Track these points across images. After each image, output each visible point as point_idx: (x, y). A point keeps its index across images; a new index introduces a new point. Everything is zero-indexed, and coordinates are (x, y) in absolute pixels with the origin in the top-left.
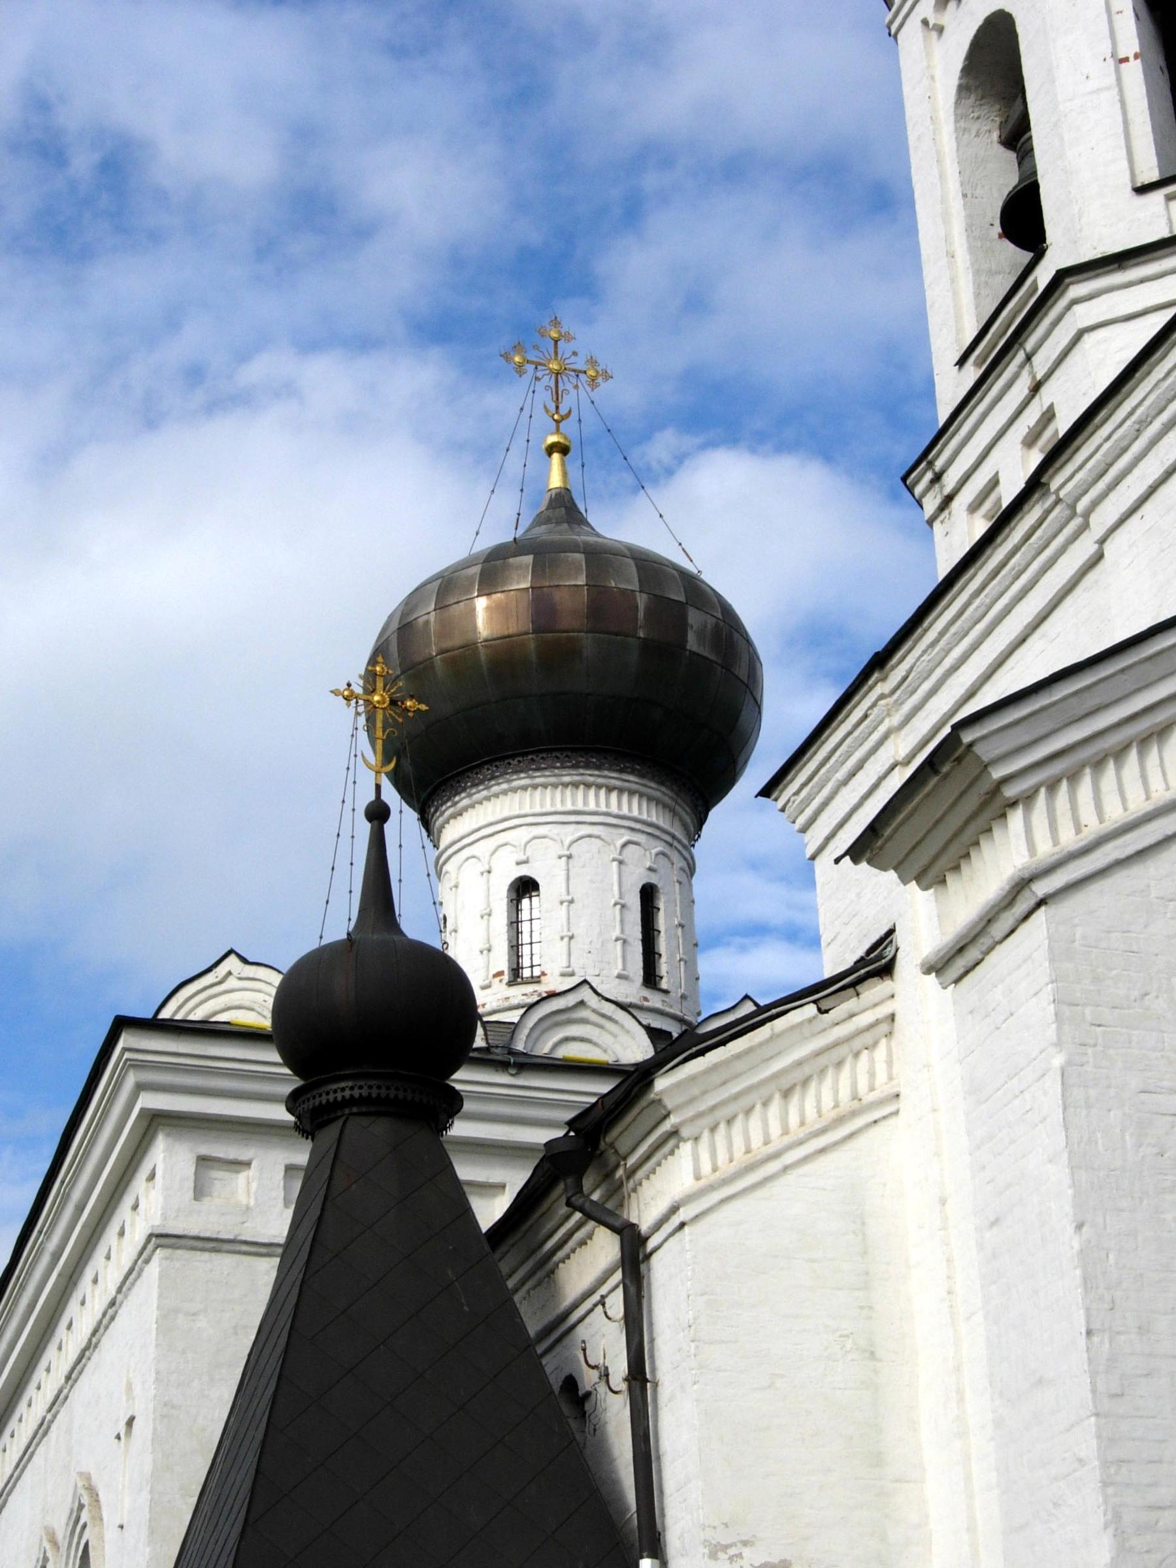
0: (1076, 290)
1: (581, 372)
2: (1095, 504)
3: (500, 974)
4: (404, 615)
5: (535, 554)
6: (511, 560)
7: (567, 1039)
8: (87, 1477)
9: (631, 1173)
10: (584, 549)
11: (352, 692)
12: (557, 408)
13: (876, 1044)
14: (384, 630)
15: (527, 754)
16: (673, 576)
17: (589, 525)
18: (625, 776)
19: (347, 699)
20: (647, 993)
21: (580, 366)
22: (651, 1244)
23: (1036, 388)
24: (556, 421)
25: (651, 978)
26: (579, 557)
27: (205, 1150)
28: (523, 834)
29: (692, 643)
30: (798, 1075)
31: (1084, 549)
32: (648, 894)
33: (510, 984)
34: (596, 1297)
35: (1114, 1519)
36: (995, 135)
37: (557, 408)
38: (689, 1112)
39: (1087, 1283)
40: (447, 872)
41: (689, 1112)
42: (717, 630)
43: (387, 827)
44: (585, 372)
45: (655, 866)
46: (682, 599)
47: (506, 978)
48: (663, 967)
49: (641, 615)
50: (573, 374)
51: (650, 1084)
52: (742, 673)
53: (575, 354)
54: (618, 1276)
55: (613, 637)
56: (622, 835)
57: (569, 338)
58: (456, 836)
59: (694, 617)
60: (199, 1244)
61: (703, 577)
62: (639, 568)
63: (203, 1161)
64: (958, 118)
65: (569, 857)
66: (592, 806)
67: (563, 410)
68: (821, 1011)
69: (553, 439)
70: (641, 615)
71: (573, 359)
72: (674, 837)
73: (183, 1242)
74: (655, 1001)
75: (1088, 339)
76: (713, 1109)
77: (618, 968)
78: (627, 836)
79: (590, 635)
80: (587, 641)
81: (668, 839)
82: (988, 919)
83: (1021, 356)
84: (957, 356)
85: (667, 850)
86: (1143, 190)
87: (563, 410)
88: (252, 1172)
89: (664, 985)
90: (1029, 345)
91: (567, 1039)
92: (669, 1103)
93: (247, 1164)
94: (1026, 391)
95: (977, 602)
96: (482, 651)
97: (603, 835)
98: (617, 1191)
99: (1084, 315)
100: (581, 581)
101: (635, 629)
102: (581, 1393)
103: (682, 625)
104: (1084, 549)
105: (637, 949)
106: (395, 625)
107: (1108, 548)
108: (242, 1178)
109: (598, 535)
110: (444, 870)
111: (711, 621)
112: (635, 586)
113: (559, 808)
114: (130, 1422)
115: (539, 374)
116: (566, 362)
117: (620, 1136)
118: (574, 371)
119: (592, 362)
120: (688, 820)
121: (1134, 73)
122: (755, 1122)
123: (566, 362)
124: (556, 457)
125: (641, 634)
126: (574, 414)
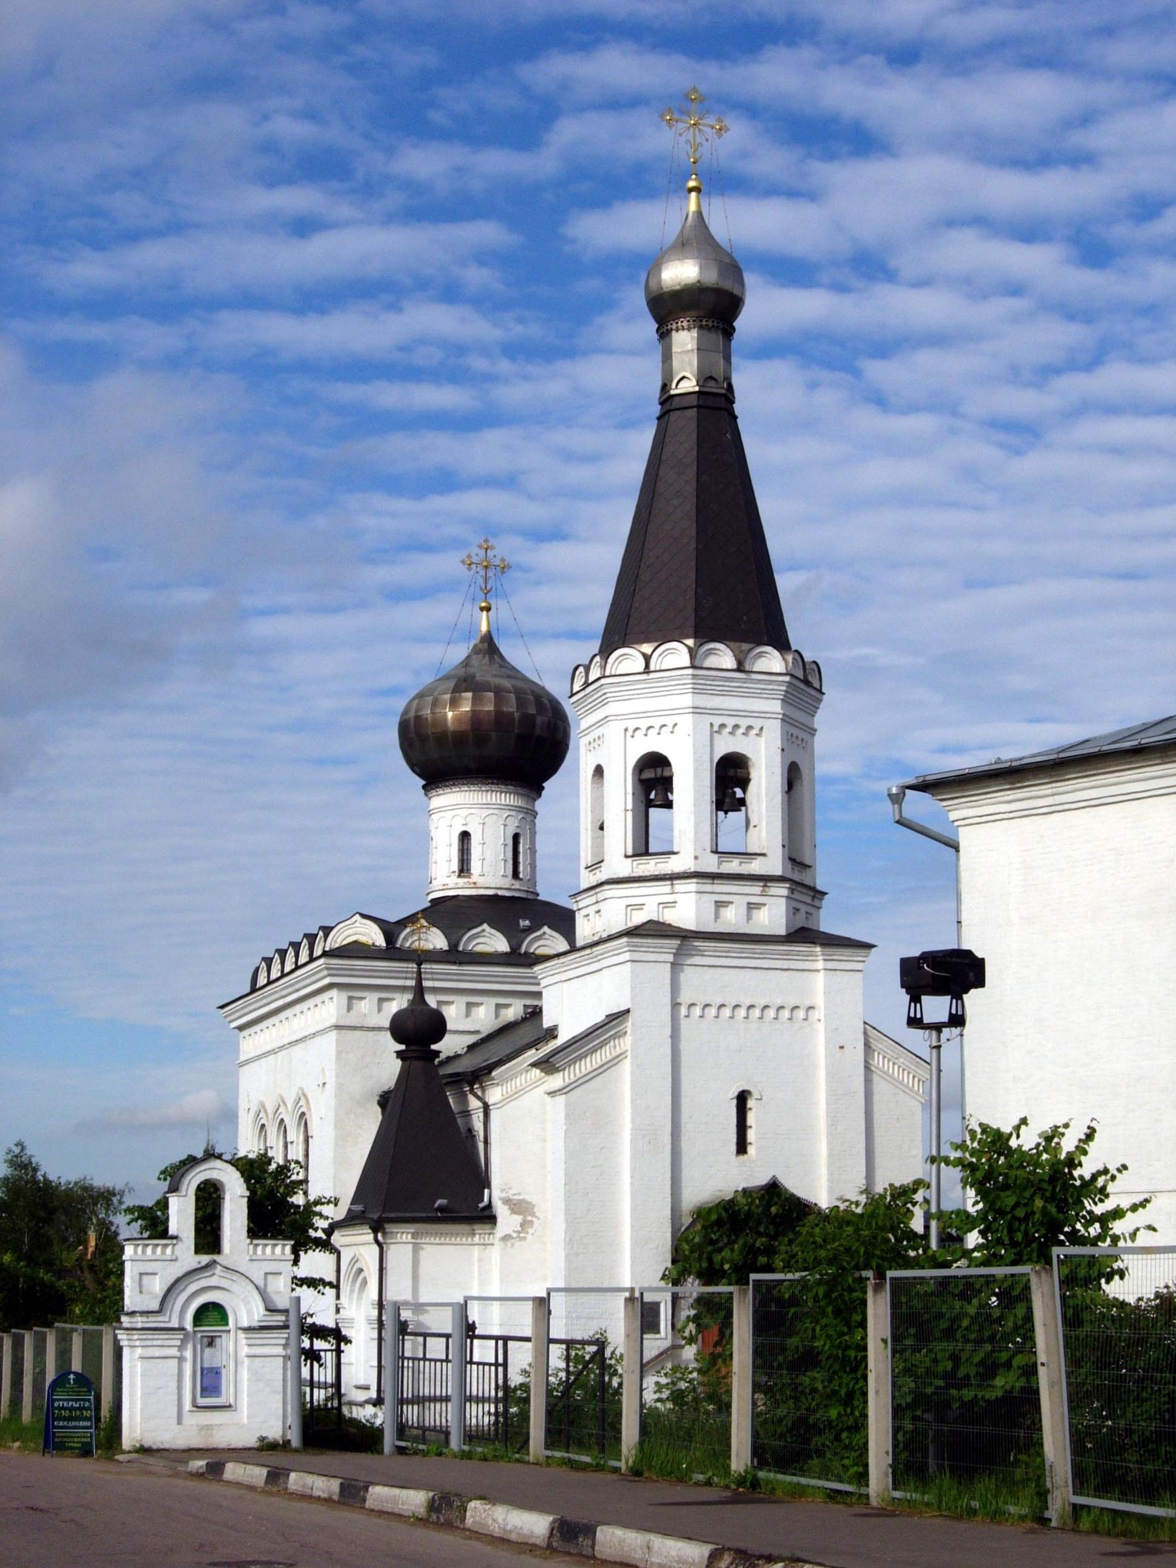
3: (454, 872)
6: (463, 694)
7: (478, 944)
8: (302, 1089)
10: (495, 687)
20: (513, 882)
25: (516, 874)
26: (491, 695)
27: (351, 994)
28: (465, 812)
29: (538, 732)
32: (516, 837)
33: (459, 876)
35: (567, 1220)
39: (566, 1174)
46: (534, 712)
47: (457, 874)
48: (521, 868)
49: (516, 723)
57: (492, 548)
62: (517, 699)
63: (350, 998)
64: (592, 783)
65: (484, 824)
66: (494, 801)
67: (488, 588)
69: (483, 604)
70: (516, 723)
74: (517, 885)
77: (502, 872)
78: (508, 813)
86: (626, 856)
87: (488, 588)
88: (367, 1001)
89: (521, 876)
91: (478, 944)
93: (365, 998)
96: (450, 739)
99: (608, 894)
100: (492, 708)
105: (510, 862)
108: (363, 1003)
111: (546, 719)
113: (480, 802)
119: (503, 560)
121: (630, 815)
122: (518, 1079)
124: (485, 613)
126: (493, 589)
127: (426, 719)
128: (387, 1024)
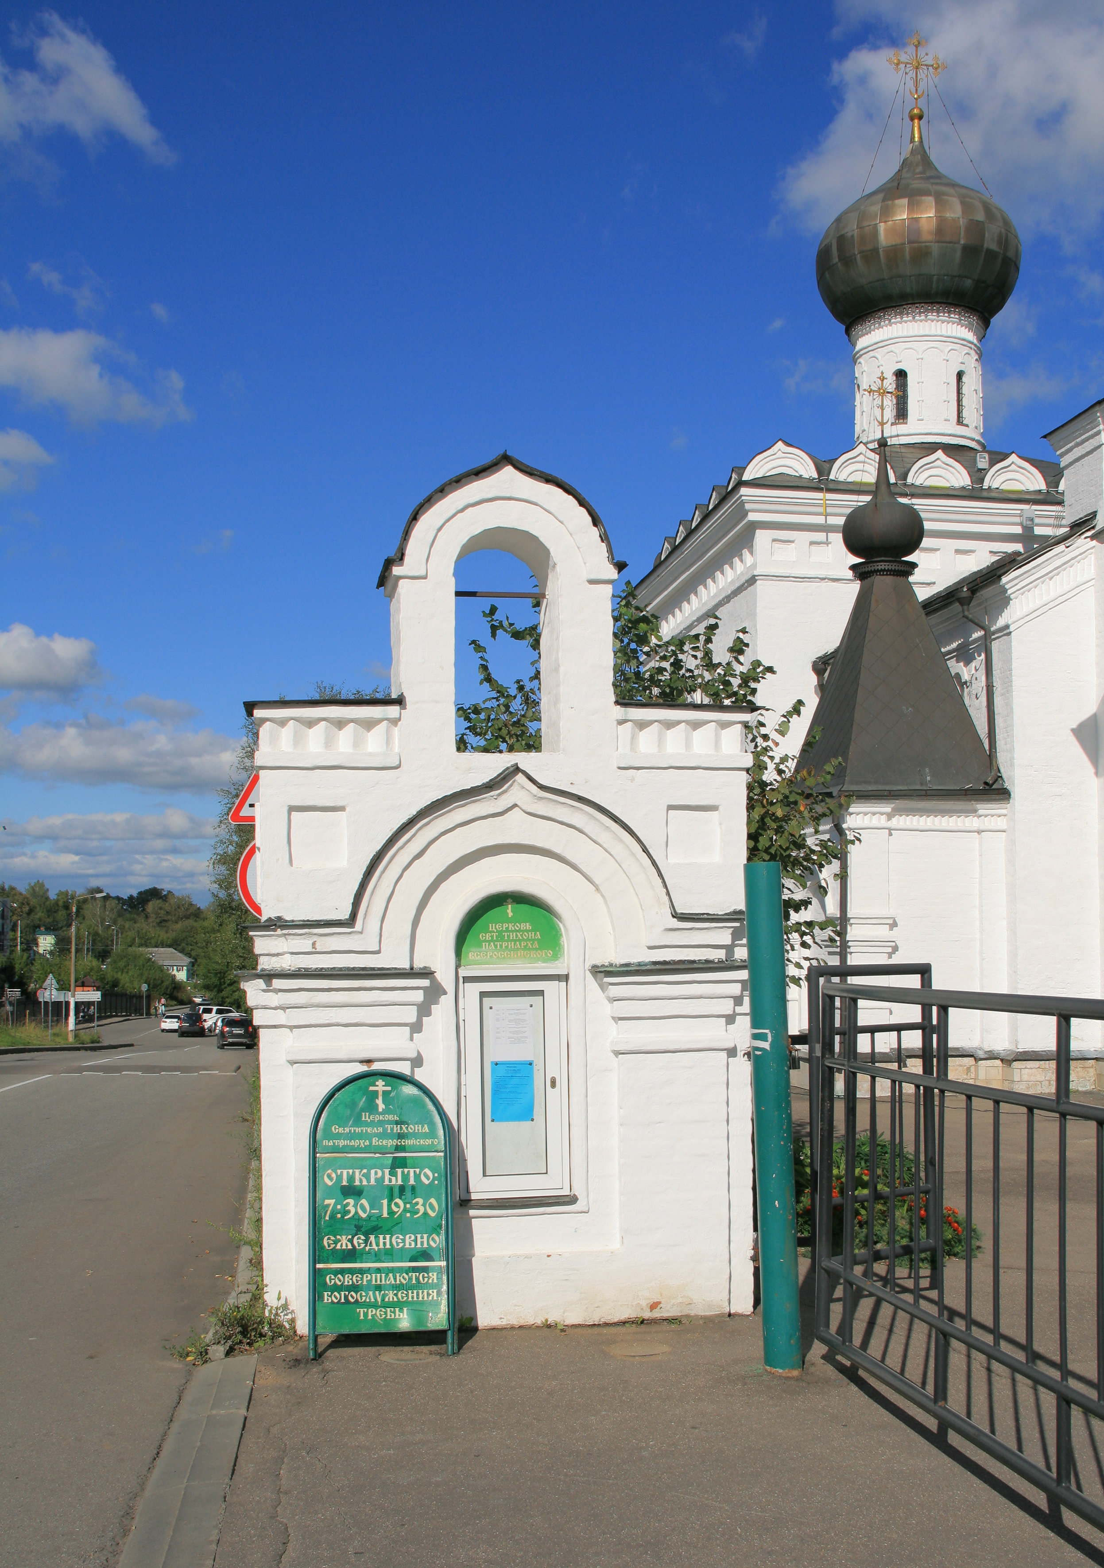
1: (930, 66)
11: (871, 390)
12: (917, 90)
15: (902, 305)
19: (869, 392)
21: (930, 62)
24: (916, 99)
25: (960, 421)
32: (960, 375)
37: (917, 90)
40: (860, 363)
44: (932, 66)
45: (963, 361)
48: (965, 414)
50: (925, 67)
51: (999, 577)
55: (948, 245)
56: (948, 346)
58: (865, 345)
67: (920, 92)
79: (936, 244)
80: (935, 249)
92: (1007, 587)
102: (963, 681)
110: (858, 361)
115: (907, 70)
116: (922, 60)
118: (926, 65)
123: (922, 60)
127: (853, 236)
128: (841, 521)
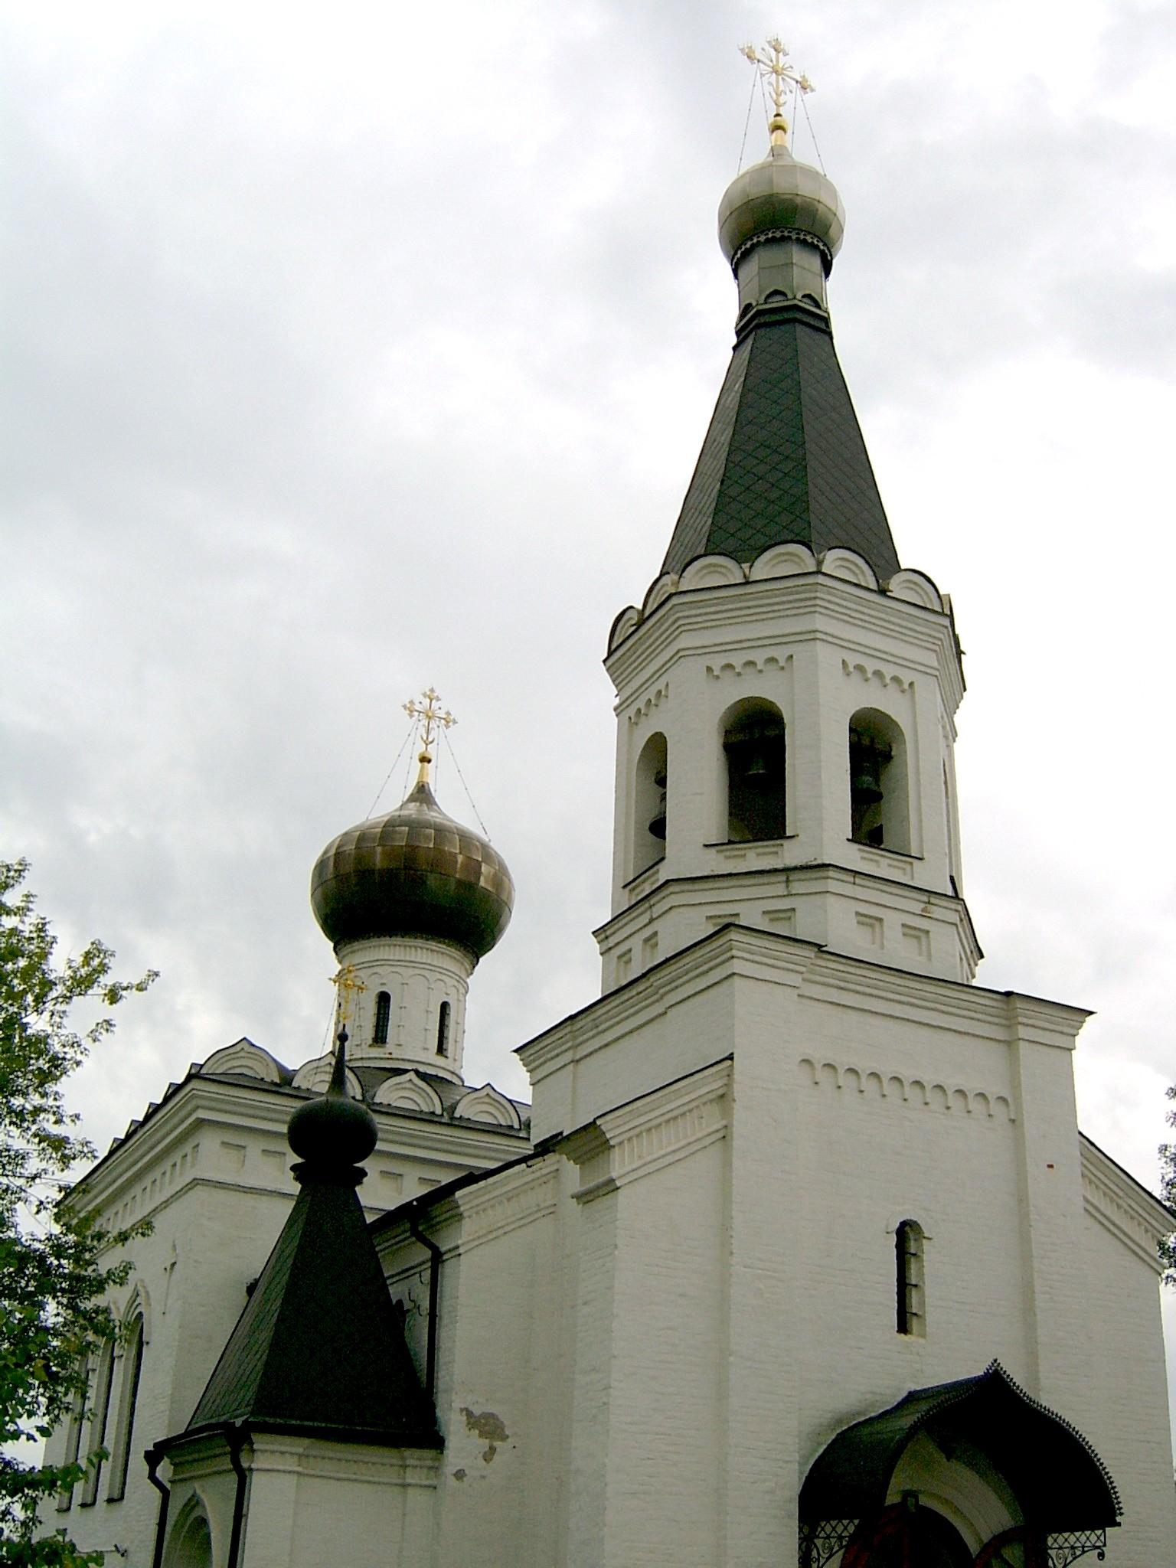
0: (672, 888)
2: (666, 993)
4: (339, 847)
5: (409, 827)
9: (439, 1223)
13: (548, 1181)
14: (325, 852)
16: (477, 846)
17: (436, 805)
18: (440, 945)
22: (445, 1257)
23: (651, 920)
30: (515, 1192)
31: (658, 1009)
34: (418, 1269)
36: (653, 779)
38: (468, 1207)
41: (468, 1207)
42: (495, 874)
43: (346, 1044)
51: (453, 1194)
52: (504, 898)
53: (440, 708)
54: (430, 1264)
59: (484, 868)
60: (218, 1185)
61: (492, 844)
68: (528, 1167)
70: (459, 866)
71: (439, 711)
72: (460, 977)
73: (210, 1183)
75: (674, 910)
76: (477, 1205)
81: (457, 978)
82: (598, 1188)
83: (647, 905)
84: (622, 885)
85: (456, 984)
90: (652, 902)
92: (460, 1203)
94: (647, 920)
95: (614, 1011)
97: (426, 975)
98: (433, 1227)
99: (674, 900)
101: (456, 872)
103: (479, 873)
104: (658, 1009)
106: (333, 851)
107: (670, 1014)
109: (441, 813)
111: (493, 871)
112: (458, 851)
114: (174, 1264)
117: (436, 1210)
119: (448, 713)
120: (468, 967)
125: (457, 876)
